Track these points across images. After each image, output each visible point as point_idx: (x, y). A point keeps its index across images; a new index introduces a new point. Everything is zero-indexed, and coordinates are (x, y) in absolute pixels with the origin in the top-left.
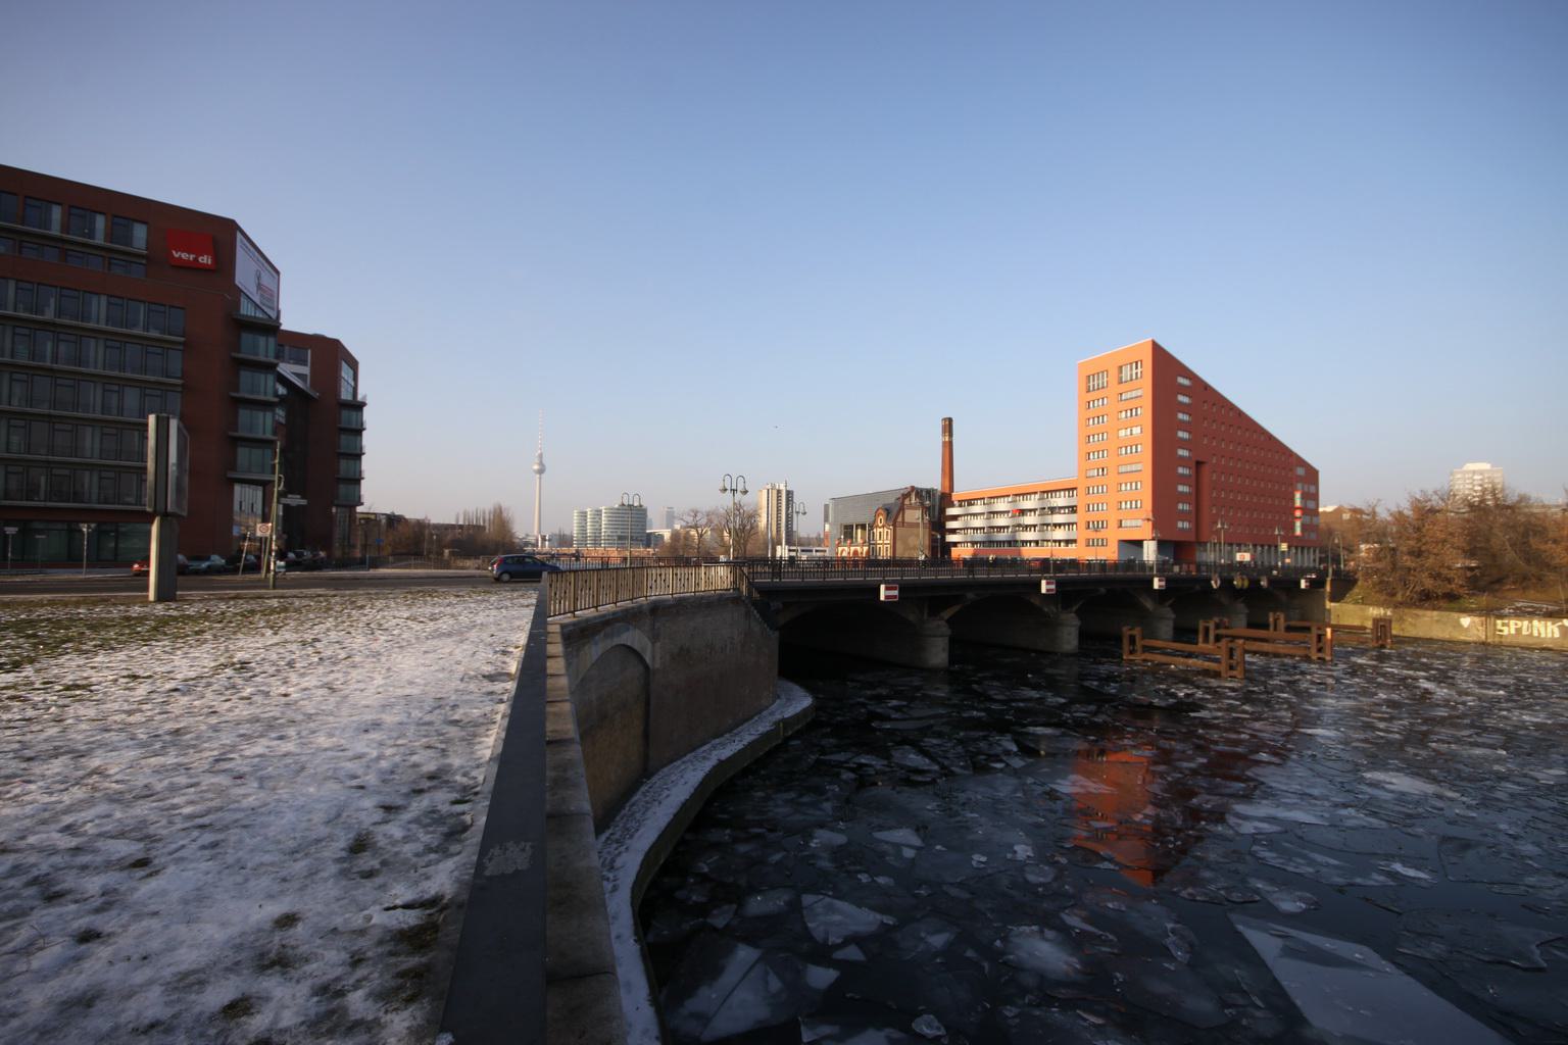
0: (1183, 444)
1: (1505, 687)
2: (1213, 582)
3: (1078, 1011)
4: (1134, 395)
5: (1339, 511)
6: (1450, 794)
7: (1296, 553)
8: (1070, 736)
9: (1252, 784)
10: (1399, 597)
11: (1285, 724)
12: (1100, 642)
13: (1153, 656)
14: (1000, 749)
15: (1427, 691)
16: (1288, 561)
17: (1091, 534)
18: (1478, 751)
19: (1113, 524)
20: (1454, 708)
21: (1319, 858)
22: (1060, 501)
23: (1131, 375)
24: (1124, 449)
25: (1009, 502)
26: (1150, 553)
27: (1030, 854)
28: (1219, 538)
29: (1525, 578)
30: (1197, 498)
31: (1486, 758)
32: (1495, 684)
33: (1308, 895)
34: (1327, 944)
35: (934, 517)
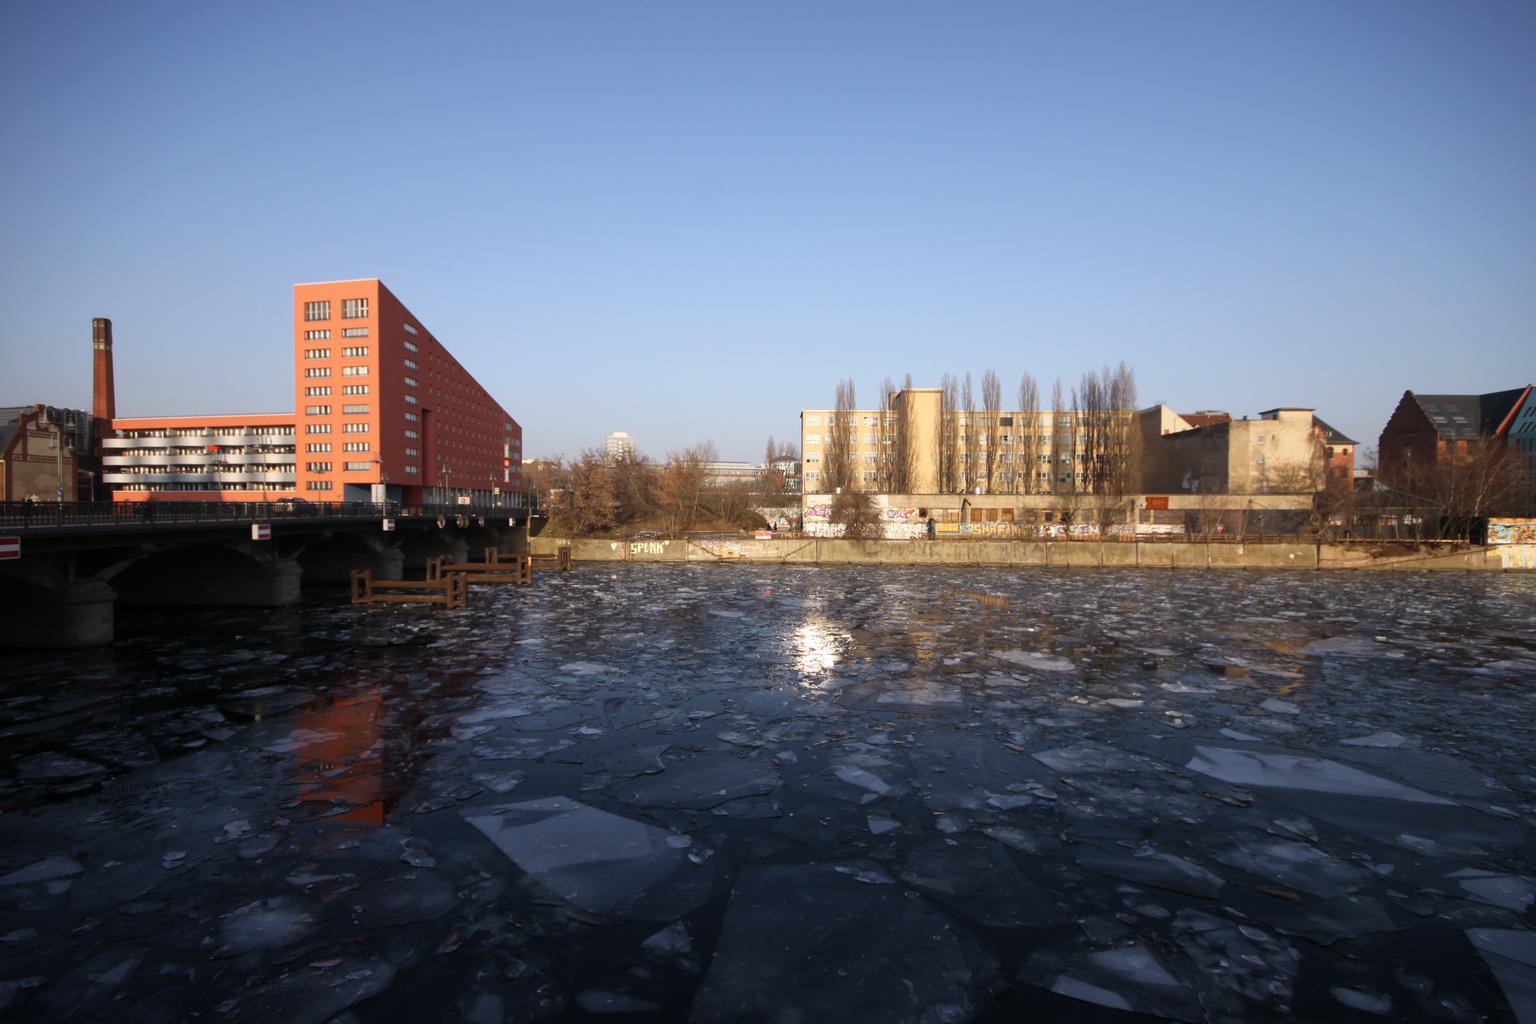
0: (411, 391)
1: (642, 589)
2: (439, 523)
3: (312, 965)
4: (360, 334)
5: (535, 464)
6: (613, 669)
7: (505, 498)
8: (296, 691)
9: (475, 696)
10: (575, 531)
11: (504, 640)
12: (325, 589)
13: (388, 600)
14: (198, 724)
15: (599, 599)
16: (499, 504)
17: (313, 477)
18: (628, 636)
19: (338, 467)
20: (615, 608)
21: (523, 741)
22: (275, 438)
23: (357, 312)
24: (349, 388)
25: (202, 436)
26: (378, 495)
27: (246, 828)
28: (444, 483)
29: (646, 514)
30: (423, 444)
31: (631, 641)
32: (636, 588)
33: (518, 772)
34: (535, 805)
35: (82, 449)
